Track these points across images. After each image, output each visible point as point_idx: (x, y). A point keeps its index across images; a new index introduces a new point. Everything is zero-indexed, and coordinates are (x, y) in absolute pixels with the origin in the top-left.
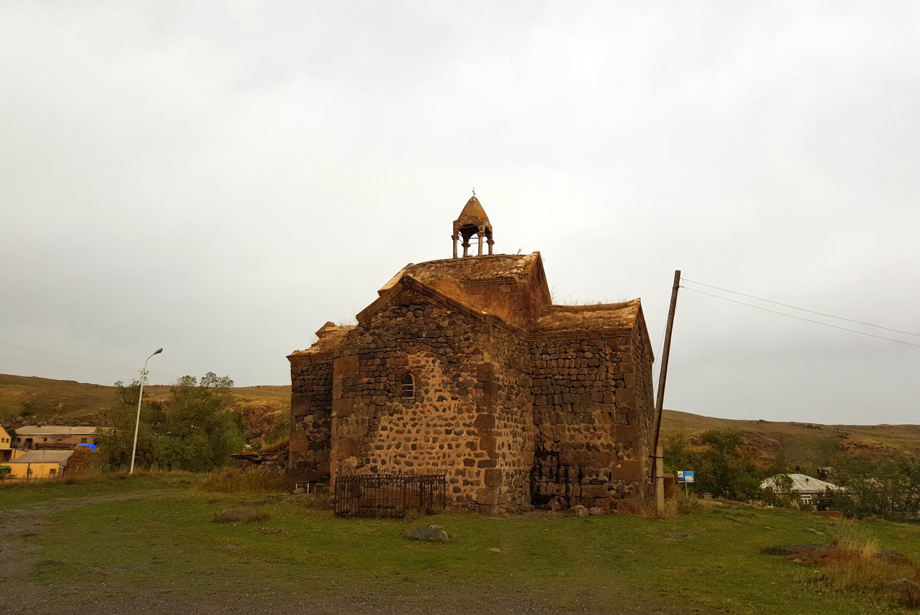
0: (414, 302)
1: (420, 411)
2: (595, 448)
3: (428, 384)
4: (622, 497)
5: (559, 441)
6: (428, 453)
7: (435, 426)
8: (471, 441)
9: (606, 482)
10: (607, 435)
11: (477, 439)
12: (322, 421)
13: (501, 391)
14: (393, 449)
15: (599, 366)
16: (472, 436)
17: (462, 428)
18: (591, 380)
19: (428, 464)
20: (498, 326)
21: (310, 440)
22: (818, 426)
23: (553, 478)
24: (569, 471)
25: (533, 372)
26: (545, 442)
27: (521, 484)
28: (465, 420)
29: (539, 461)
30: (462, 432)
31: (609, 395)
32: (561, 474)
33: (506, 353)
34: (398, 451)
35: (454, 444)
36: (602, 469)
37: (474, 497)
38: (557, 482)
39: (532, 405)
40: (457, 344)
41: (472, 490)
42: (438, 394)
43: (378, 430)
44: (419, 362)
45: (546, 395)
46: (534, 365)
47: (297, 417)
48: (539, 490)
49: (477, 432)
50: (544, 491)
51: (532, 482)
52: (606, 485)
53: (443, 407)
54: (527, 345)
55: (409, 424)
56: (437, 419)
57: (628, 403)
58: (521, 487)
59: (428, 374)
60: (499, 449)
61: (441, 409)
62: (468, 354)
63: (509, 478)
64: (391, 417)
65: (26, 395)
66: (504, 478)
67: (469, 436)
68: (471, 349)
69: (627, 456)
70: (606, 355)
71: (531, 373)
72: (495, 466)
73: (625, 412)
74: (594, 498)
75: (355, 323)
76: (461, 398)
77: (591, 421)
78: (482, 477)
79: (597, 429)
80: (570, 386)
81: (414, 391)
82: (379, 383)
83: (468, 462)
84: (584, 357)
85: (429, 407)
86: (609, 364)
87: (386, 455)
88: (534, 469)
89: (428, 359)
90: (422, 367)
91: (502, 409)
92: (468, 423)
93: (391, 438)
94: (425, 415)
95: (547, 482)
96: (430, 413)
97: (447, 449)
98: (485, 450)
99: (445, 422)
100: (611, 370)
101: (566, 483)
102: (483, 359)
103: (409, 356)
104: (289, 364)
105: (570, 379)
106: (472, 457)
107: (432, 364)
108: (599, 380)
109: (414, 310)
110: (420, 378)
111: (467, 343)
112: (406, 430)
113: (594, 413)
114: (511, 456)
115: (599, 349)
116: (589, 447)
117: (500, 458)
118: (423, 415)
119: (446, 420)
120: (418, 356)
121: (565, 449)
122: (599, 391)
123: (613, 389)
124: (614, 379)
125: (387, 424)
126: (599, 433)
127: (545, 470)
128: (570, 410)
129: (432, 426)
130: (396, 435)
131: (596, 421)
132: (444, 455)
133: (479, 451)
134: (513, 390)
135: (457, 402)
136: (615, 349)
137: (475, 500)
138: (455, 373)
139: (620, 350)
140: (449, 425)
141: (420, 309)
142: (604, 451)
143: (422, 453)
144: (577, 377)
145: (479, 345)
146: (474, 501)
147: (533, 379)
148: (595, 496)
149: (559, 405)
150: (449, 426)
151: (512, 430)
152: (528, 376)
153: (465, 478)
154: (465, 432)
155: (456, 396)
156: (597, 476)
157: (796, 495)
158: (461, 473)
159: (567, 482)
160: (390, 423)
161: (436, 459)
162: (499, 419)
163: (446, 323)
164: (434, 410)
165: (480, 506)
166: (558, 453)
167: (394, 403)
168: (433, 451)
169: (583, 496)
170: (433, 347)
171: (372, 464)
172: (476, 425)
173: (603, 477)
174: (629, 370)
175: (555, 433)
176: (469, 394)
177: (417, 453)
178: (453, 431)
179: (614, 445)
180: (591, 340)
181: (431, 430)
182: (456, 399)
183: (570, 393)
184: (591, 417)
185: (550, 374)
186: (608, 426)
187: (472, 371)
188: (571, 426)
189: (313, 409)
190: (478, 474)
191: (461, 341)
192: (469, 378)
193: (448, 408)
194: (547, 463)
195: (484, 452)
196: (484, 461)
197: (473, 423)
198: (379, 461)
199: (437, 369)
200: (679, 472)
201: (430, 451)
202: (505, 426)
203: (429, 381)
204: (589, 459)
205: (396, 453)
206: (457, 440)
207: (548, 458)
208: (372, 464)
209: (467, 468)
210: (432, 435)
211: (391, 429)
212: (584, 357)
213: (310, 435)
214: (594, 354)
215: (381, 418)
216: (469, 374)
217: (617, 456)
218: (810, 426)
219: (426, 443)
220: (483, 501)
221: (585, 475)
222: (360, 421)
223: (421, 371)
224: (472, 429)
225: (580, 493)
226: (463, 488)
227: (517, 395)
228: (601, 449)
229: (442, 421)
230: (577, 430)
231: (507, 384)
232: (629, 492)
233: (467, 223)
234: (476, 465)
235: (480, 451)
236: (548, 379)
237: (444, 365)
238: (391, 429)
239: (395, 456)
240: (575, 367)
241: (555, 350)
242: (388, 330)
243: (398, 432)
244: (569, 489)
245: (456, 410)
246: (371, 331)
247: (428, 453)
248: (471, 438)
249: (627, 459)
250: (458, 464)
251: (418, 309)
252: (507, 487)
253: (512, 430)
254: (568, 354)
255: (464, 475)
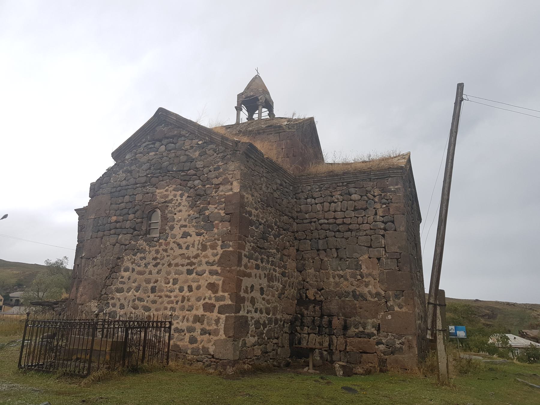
2: (362, 297)
3: (174, 220)
4: (393, 353)
5: (323, 289)
6: (167, 296)
7: (177, 265)
8: (212, 282)
9: (374, 335)
10: (375, 283)
11: (220, 280)
13: (253, 228)
14: (133, 292)
15: (367, 208)
16: (215, 277)
17: (204, 267)
18: (357, 224)
19: (166, 308)
20: (253, 157)
22: (513, 304)
23: (315, 329)
24: (333, 322)
25: (297, 217)
26: (308, 289)
27: (276, 335)
29: (301, 310)
31: (377, 238)
32: (324, 325)
33: (264, 189)
35: (194, 285)
36: (369, 320)
37: (211, 350)
38: (320, 333)
39: (295, 251)
40: (206, 175)
41: (209, 341)
42: (183, 229)
44: (167, 196)
45: (310, 240)
46: (299, 210)
48: (300, 343)
49: (219, 271)
50: (305, 344)
51: (292, 333)
52: (374, 339)
53: (187, 244)
54: (291, 189)
55: (151, 264)
56: (180, 258)
57: (399, 247)
58: (277, 338)
59: (175, 209)
60: (246, 291)
61: (184, 246)
62: (217, 185)
63: (260, 328)
64: (134, 257)
65: (22, 273)
66: (252, 328)
67: (211, 277)
68: (221, 179)
69: (399, 306)
70: (374, 196)
71: (295, 218)
72: (239, 312)
73: (395, 257)
74: (361, 353)
75: (112, 163)
76: (206, 233)
77: (358, 267)
79: (365, 275)
80: (335, 230)
82: (127, 221)
83: (208, 307)
84: (351, 200)
85: (172, 245)
86: (378, 206)
88: (296, 319)
89: (176, 193)
90: (171, 201)
91: (253, 247)
92: (211, 261)
94: (168, 254)
95: (309, 334)
97: (186, 292)
98: (227, 292)
100: (380, 212)
101: (329, 335)
102: (231, 189)
103: (158, 191)
104: (77, 216)
105: (335, 223)
106: (213, 301)
108: (367, 223)
109: (167, 144)
110: (167, 214)
111: (216, 173)
112: (147, 270)
113: (361, 258)
114: (263, 302)
115: (367, 191)
116: (355, 296)
117: (247, 303)
118: (165, 254)
119: (188, 258)
122: (366, 235)
123: (382, 232)
124: (383, 222)
126: (367, 280)
127: (307, 320)
128: (336, 256)
129: (173, 266)
130: (137, 276)
131: (364, 267)
132: (183, 298)
133: (220, 293)
134: (270, 230)
135: (202, 237)
136: (384, 190)
137: (212, 353)
138: (202, 206)
139: (390, 191)
140: (192, 264)
142: (372, 300)
143: (160, 297)
144: (343, 221)
145: (229, 174)
146: (210, 355)
147: (297, 224)
148: (361, 351)
149: (323, 250)
151: (266, 273)
152: (291, 220)
153: (203, 326)
154: (207, 272)
155: (201, 232)
157: (511, 349)
158: (198, 319)
159: (330, 335)
160: (132, 263)
162: (250, 257)
163: (197, 153)
164: (178, 247)
165: (218, 360)
166: (321, 301)
167: (138, 242)
168: (172, 294)
169: (348, 350)
170: (182, 180)
172: (220, 264)
173: (370, 329)
174: (400, 212)
176: (215, 229)
177: (155, 296)
178: (195, 271)
179: (383, 293)
180: (359, 182)
181: (172, 269)
183: (335, 237)
184: (358, 263)
185: (315, 218)
186: (376, 272)
187: (220, 203)
190: (217, 321)
191: (210, 171)
192: (216, 211)
193: (191, 246)
194: (310, 312)
195: (226, 294)
196: (225, 305)
197: (216, 261)
199: (184, 203)
200: (450, 327)
201: (169, 294)
202: (257, 267)
203: (175, 217)
204: (355, 308)
205: (135, 296)
206: (198, 282)
207: (311, 307)
209: (205, 314)
212: (351, 200)
214: (361, 196)
215: (125, 258)
216: (216, 206)
217: (387, 305)
218: (508, 304)
219: (166, 285)
220: (220, 355)
221: (351, 326)
223: (168, 206)
224: (215, 268)
225: (344, 347)
226: (199, 338)
227: (275, 236)
228: (369, 298)
229: (184, 260)
230: (342, 276)
231: (263, 222)
232: (401, 348)
234: (216, 310)
236: (313, 224)
237: (191, 198)
238: (133, 270)
239: (134, 300)
240: (341, 211)
241: (321, 194)
242: (140, 166)
243: (141, 273)
244: (332, 342)
245: (200, 246)
246: (125, 168)
247: (167, 296)
248: (214, 279)
249: (399, 310)
250: (197, 309)
251: (170, 143)
252: (256, 338)
253: (266, 273)
254: (334, 198)
255: (202, 322)
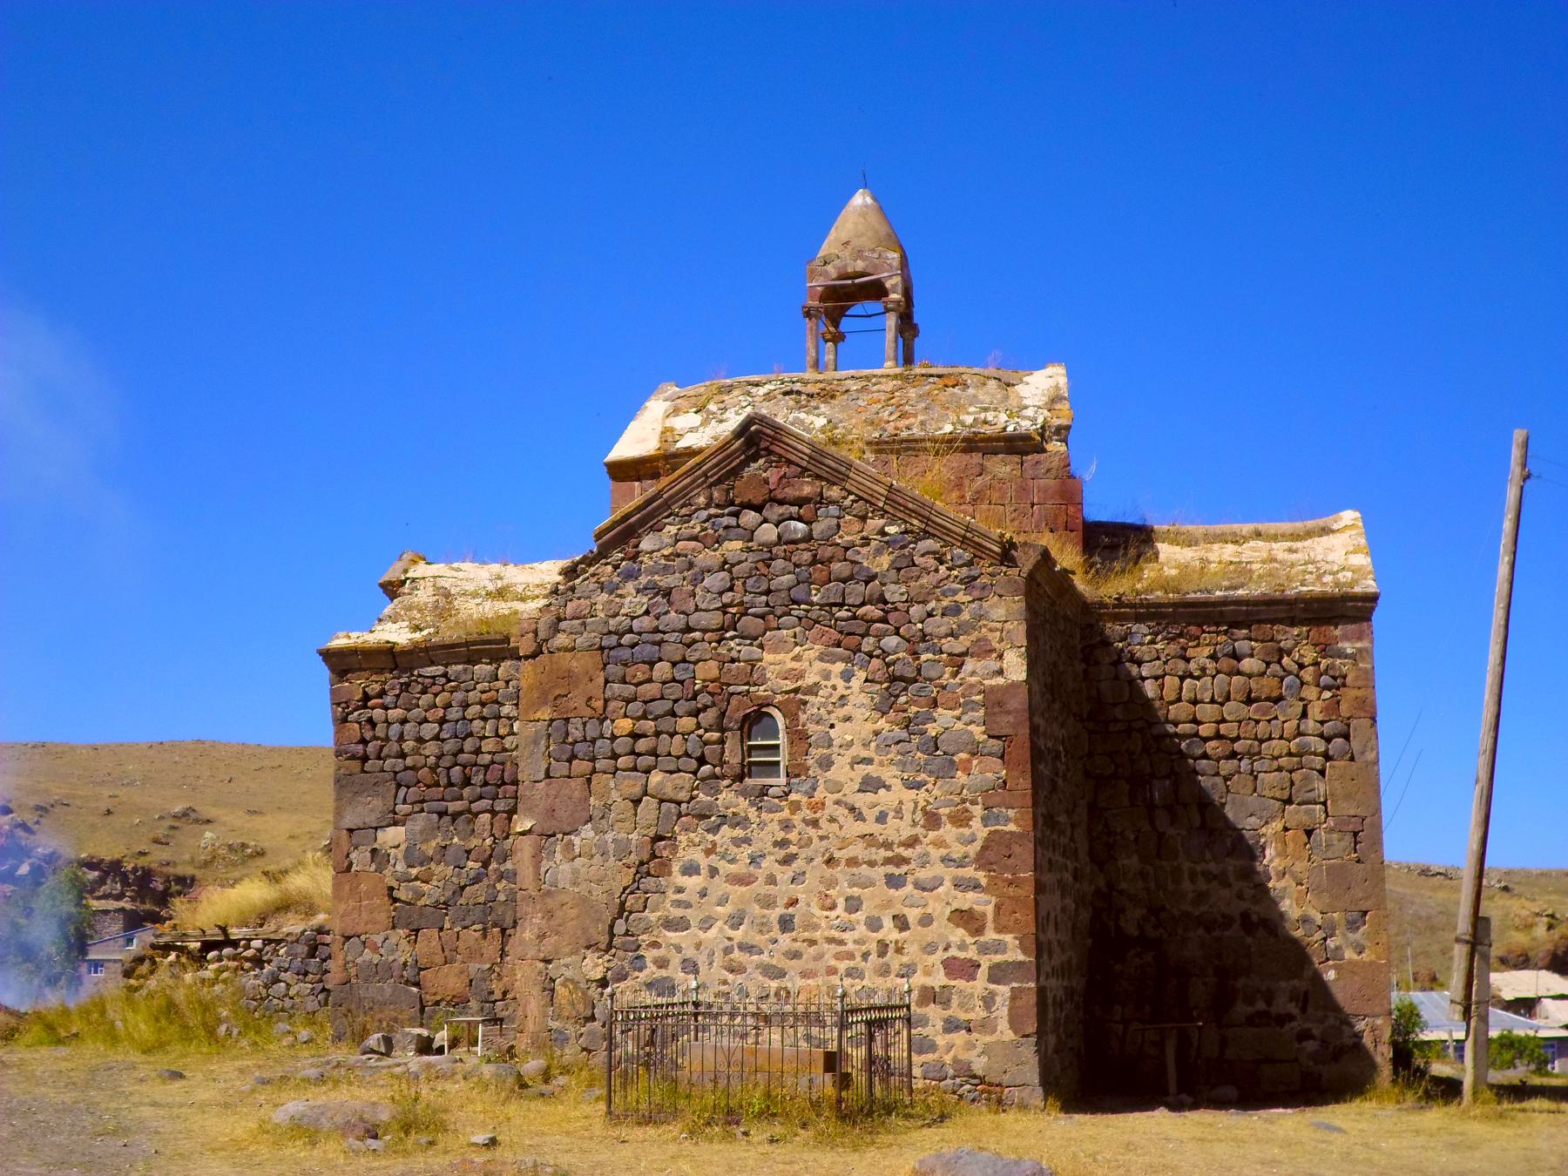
0: (779, 495)
1: (804, 820)
6: (831, 940)
7: (853, 862)
9: (1291, 1018)
12: (433, 844)
14: (721, 930)
17: (938, 869)
19: (832, 971)
21: (395, 900)
28: (947, 847)
30: (939, 882)
34: (738, 935)
35: (913, 915)
36: (1283, 984)
42: (863, 770)
43: (670, 874)
47: (351, 831)
49: (984, 882)
56: (861, 844)
64: (710, 837)
78: (1002, 1011)
81: (783, 758)
86: (1310, 693)
87: (698, 946)
90: (813, 690)
93: (714, 896)
96: (835, 826)
98: (1011, 933)
99: (883, 853)
100: (1315, 711)
103: (768, 657)
106: (972, 953)
107: (840, 684)
111: (951, 622)
118: (812, 832)
119: (887, 845)
120: (797, 658)
121: (1180, 931)
124: (1321, 736)
125: (697, 856)
129: (843, 863)
132: (883, 947)
135: (922, 794)
141: (800, 519)
143: (812, 942)
145: (991, 630)
150: (898, 866)
153: (947, 1013)
156: (1269, 1003)
160: (708, 852)
161: (858, 959)
163: (885, 561)
168: (846, 936)
171: (651, 972)
172: (982, 861)
173: (1284, 1005)
175: (1152, 885)
177: (795, 940)
178: (910, 878)
179: (1318, 918)
182: (918, 786)
188: (1199, 868)
189: (402, 809)
193: (892, 814)
195: (1008, 938)
198: (676, 960)
205: (730, 939)
208: (651, 972)
209: (953, 983)
210: (838, 894)
211: (713, 872)
213: (395, 884)
215: (679, 838)
219: (826, 913)
222: (611, 847)
224: (969, 872)
226: (941, 1041)
230: (1215, 877)
233: (850, 270)
234: (982, 973)
235: (996, 936)
239: (727, 951)
245: (919, 816)
246: (643, 580)
249: (1355, 957)
251: (791, 518)
